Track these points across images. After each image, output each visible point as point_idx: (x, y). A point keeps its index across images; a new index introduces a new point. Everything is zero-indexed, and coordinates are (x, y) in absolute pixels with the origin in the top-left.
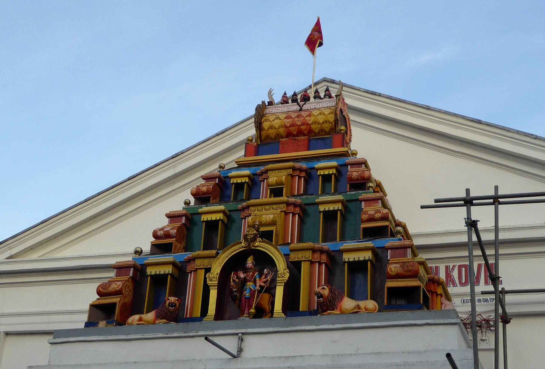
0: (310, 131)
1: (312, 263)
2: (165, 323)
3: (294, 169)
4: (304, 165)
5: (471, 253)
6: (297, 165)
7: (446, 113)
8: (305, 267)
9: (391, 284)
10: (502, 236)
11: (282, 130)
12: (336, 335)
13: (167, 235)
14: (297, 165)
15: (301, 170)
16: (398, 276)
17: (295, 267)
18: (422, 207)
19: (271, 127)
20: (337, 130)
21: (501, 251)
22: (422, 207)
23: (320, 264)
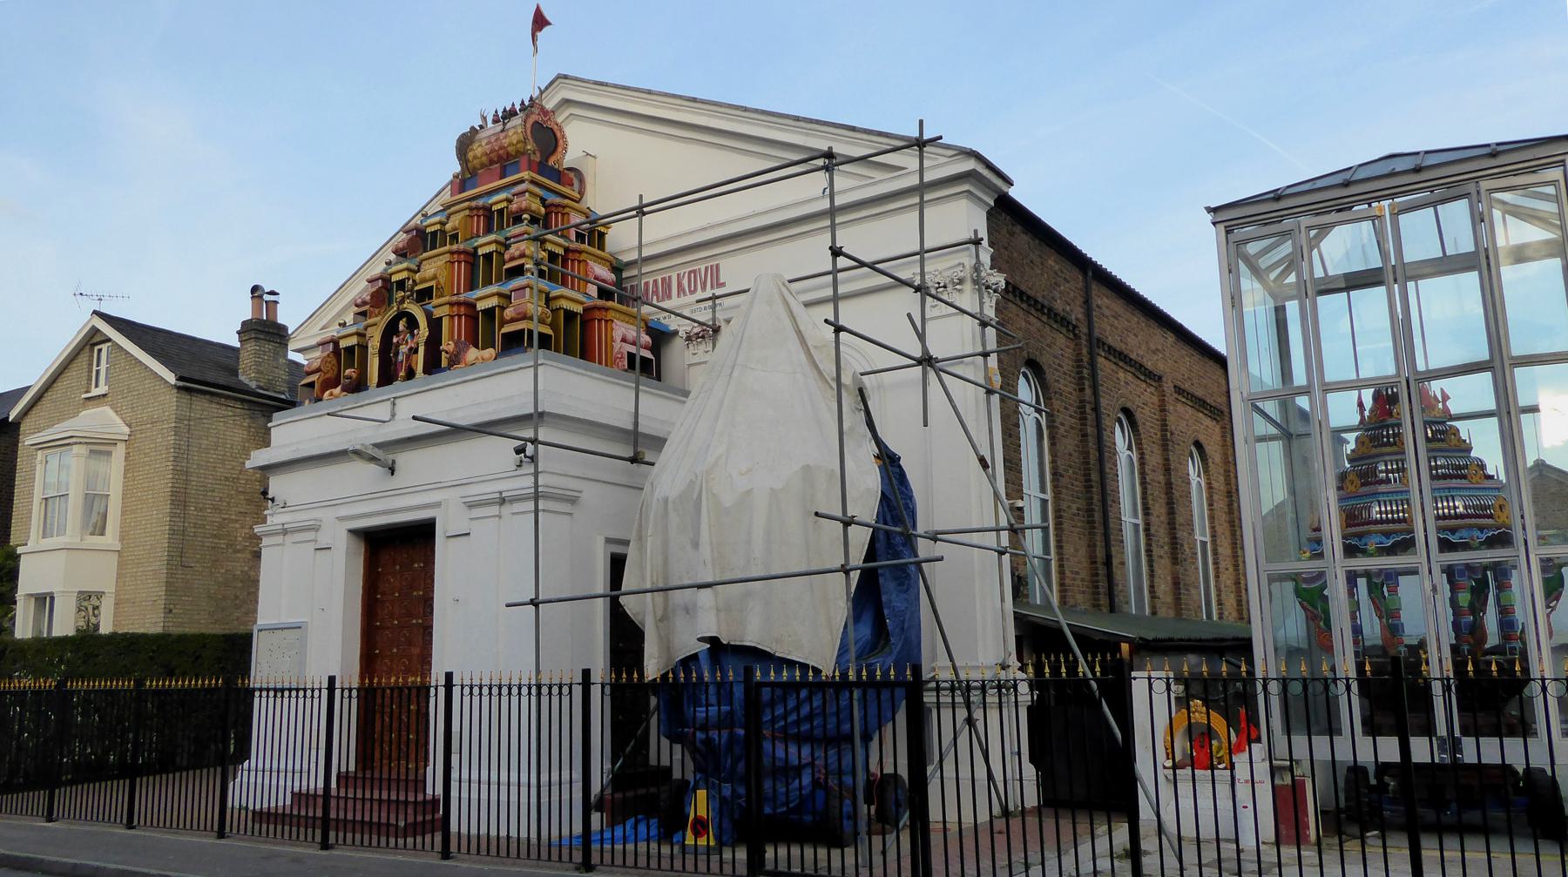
0: (500, 157)
1: (452, 317)
2: (1361, 405)
3: (471, 209)
4: (480, 202)
5: (833, 221)
6: (474, 204)
7: (666, 95)
8: (445, 322)
9: (507, 329)
10: (839, 201)
11: (484, 159)
12: (618, 388)
13: (364, 303)
14: (474, 204)
15: (477, 208)
16: (513, 320)
17: (435, 325)
18: (921, 122)
19: (475, 157)
20: (547, 138)
21: (838, 220)
22: (921, 122)
23: (460, 316)
